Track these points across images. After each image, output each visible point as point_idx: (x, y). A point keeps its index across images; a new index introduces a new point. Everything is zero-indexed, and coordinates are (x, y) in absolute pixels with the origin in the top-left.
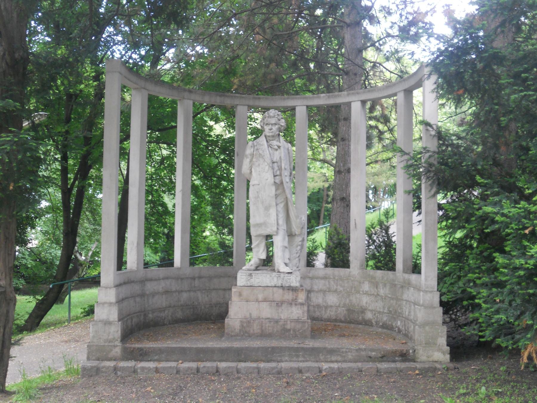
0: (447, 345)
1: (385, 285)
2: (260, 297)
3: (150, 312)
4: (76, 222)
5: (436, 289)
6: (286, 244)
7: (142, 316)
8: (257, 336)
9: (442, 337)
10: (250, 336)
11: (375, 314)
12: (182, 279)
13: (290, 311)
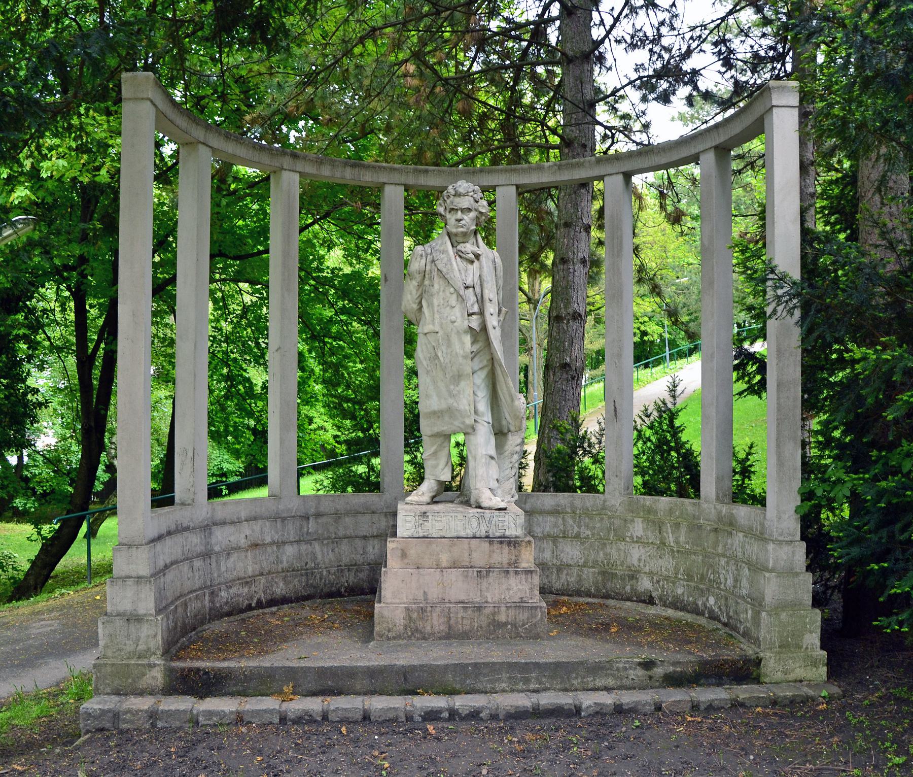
0: (822, 648)
1: (677, 526)
2: (445, 559)
3: (223, 587)
4: (103, 412)
5: (798, 537)
6: (493, 452)
7: (207, 597)
8: (440, 638)
9: (811, 632)
10: (424, 638)
11: (658, 582)
12: (284, 519)
13: (504, 587)
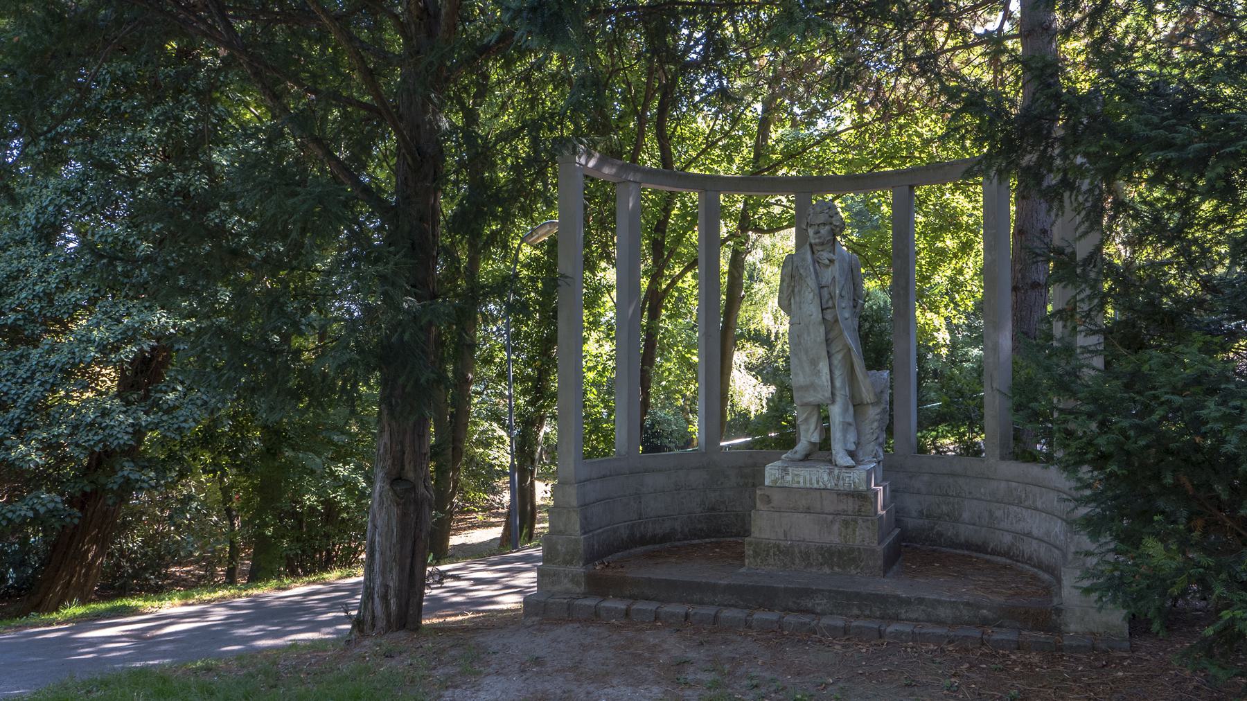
6: (850, 419)
